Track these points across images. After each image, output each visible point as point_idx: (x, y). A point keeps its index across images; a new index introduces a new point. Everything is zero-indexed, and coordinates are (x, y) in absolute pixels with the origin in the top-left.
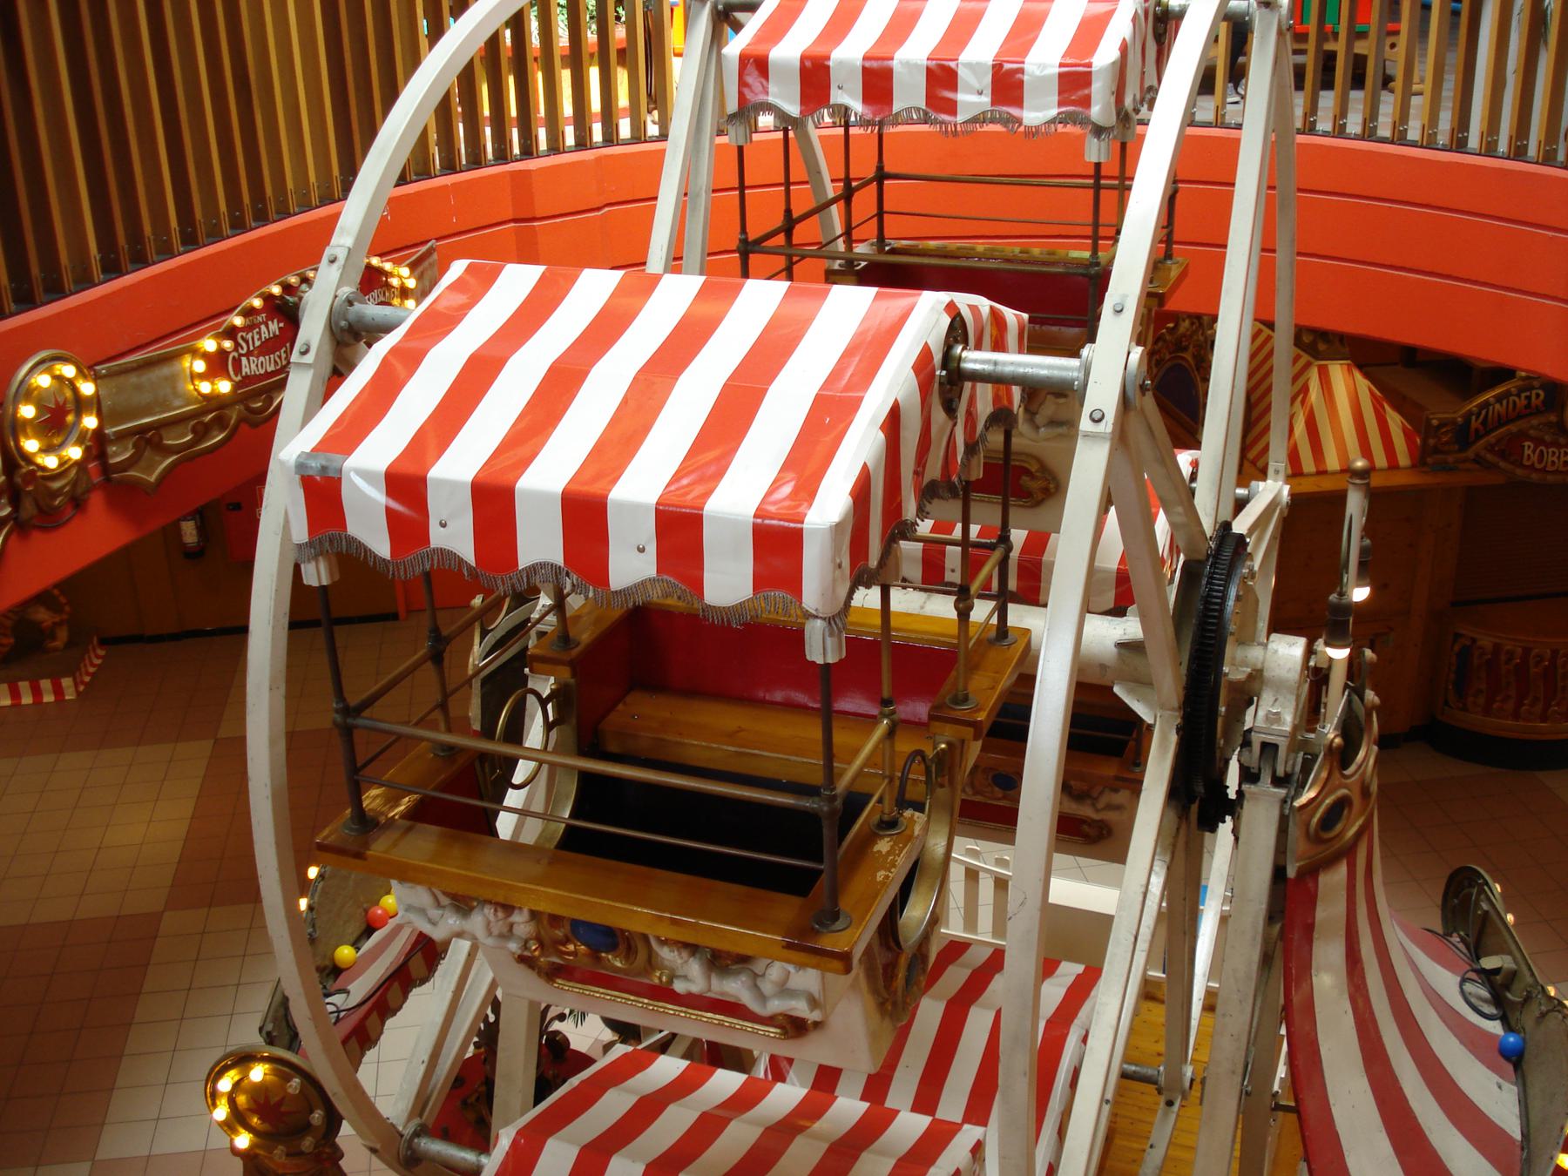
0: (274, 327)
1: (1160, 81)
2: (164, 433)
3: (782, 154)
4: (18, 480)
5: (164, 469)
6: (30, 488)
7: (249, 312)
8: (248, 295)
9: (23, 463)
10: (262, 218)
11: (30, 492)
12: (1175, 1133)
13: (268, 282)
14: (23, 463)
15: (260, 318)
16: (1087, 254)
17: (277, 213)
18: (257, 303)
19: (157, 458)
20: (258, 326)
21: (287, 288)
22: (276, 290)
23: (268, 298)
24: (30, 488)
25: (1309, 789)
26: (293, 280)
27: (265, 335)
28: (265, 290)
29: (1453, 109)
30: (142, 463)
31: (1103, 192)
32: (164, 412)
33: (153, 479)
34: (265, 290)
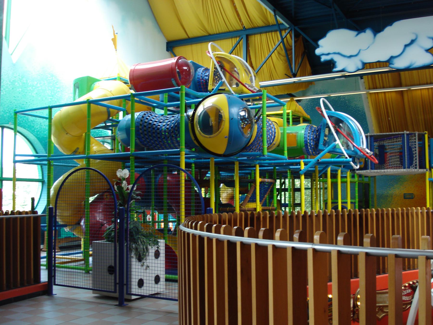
0: (410, 291)
1: (426, 277)
2: (384, 308)
3: (72, 288)
4: (355, 310)
5: (383, 316)
6: (357, 312)
7: (405, 286)
8: (405, 283)
9: (356, 307)
10: (409, 269)
11: (357, 313)
12: (368, 64)
13: (410, 281)
14: (356, 307)
15: (407, 288)
16: (104, 125)
17: (413, 268)
18: (407, 285)
19: (382, 313)
20: (406, 290)
21: (414, 283)
22: (411, 283)
23: (409, 284)
24: (357, 312)
25: (216, 68)
26: (415, 281)
27: (407, 292)
28: (408, 282)
29: (47, 261)
30: (379, 314)
31: (18, 176)
32: (385, 304)
33: (380, 317)
34: (408, 282)
